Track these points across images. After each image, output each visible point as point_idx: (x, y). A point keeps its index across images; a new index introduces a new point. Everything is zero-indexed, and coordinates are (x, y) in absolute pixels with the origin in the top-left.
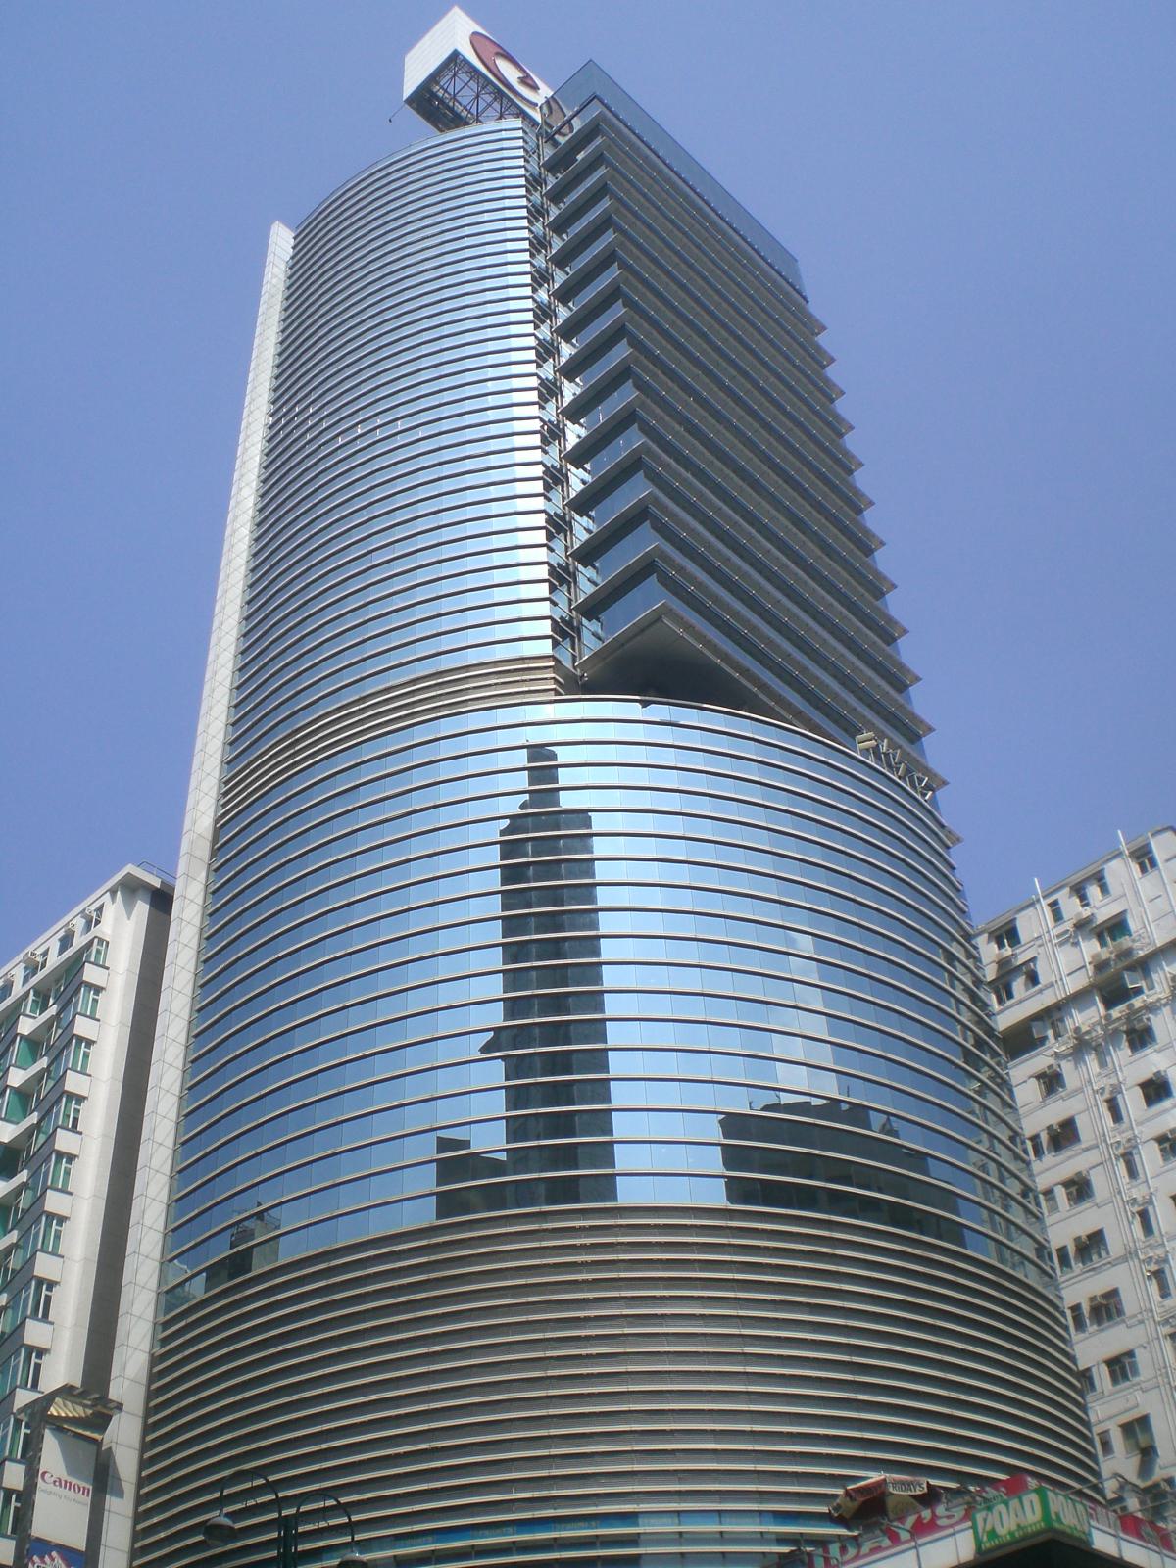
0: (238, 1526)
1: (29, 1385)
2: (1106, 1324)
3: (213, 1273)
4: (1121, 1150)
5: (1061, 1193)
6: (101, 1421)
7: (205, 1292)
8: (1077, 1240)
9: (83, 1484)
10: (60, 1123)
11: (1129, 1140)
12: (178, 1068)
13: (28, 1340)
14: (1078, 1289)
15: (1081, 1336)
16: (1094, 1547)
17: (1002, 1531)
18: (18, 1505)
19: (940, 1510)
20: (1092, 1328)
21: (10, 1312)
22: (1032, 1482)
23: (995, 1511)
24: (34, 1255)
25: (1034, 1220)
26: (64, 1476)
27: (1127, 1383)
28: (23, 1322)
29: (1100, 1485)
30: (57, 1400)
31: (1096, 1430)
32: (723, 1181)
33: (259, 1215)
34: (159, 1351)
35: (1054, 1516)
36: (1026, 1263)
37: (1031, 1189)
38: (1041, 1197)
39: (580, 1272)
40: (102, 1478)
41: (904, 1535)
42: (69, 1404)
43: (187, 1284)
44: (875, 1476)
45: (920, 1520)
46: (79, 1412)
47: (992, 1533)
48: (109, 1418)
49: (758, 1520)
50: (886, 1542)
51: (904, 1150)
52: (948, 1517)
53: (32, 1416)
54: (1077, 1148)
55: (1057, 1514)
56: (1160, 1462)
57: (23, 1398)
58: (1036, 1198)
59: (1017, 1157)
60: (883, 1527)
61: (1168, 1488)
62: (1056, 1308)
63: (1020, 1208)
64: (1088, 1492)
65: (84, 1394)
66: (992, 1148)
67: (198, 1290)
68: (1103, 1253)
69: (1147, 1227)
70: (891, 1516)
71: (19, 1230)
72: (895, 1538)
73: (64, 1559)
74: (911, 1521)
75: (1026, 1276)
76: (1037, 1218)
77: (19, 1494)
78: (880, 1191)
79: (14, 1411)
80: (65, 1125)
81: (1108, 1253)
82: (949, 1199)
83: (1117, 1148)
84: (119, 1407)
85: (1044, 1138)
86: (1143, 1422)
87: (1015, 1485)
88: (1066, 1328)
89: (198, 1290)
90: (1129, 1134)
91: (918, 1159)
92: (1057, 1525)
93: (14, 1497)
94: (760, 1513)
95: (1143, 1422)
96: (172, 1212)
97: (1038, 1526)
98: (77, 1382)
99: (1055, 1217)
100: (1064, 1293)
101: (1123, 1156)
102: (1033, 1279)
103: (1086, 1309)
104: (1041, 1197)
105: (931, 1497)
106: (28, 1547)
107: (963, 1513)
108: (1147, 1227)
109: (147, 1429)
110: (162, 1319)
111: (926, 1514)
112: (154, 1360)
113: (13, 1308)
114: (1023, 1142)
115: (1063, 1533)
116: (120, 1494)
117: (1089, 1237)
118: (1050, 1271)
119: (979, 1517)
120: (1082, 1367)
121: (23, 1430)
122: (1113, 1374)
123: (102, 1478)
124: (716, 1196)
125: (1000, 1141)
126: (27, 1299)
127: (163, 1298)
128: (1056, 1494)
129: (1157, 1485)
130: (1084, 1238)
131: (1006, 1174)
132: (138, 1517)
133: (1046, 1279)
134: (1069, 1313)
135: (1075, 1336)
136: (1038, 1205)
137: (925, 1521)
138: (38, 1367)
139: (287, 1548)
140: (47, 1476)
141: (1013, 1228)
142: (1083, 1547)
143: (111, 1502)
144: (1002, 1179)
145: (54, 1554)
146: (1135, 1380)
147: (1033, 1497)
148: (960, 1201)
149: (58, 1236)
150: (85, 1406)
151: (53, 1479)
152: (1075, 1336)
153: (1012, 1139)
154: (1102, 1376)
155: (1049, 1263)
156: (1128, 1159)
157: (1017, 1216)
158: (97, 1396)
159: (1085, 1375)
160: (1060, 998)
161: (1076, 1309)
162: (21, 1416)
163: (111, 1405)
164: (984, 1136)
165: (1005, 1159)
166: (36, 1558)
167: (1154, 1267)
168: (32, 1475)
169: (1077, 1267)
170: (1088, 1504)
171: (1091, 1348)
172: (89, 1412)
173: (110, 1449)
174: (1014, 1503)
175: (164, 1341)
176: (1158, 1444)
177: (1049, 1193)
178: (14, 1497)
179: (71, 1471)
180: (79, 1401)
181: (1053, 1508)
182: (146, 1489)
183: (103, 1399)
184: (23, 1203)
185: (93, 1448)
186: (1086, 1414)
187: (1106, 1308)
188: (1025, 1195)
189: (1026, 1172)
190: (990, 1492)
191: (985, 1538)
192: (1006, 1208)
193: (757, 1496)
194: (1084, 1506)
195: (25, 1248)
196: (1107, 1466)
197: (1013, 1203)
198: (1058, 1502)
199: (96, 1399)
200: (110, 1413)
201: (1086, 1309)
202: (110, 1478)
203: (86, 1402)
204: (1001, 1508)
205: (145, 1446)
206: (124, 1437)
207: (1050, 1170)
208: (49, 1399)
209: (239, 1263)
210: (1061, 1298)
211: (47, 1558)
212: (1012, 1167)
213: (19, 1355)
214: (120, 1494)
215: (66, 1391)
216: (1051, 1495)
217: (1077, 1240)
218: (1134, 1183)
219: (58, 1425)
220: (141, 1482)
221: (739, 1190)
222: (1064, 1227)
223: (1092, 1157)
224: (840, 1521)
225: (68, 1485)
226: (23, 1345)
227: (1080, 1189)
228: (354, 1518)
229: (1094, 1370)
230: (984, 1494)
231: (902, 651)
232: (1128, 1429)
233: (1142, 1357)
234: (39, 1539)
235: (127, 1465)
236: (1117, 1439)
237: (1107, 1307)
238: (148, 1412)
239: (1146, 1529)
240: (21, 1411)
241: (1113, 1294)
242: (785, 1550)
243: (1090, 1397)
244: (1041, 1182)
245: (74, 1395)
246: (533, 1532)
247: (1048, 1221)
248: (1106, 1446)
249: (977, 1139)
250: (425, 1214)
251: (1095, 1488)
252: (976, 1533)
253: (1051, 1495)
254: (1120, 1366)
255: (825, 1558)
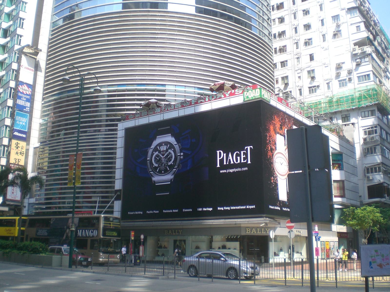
0: (71, 80)
1: (18, 44)
2: (282, 53)
3: (65, 19)
4: (293, 12)
5: (277, 20)
6: (36, 54)
7: (63, 23)
8: (279, 32)
9: (32, 68)
10: (10, 79)
11: (296, 10)
12: (46, 45)
13: (18, 33)
14: (277, 44)
15: (276, 55)
16: (270, 103)
17: (249, 97)
18: (16, 73)
19: (236, 90)
20: (278, 54)
21: (13, 26)
22: (259, 87)
23: (249, 92)
24: (19, 12)
25: (269, 26)
26: (27, 66)
27: (285, 68)
28: (17, 28)
29: (274, 90)
30: (25, 48)
31: (275, 77)
32: (195, 7)
33: (77, 5)
34: (51, 37)
35: (262, 95)
36: (266, 36)
37: (271, 33)
38: (272, 21)
39: (157, 40)
40: (37, 67)
41: (227, 95)
42: (28, 49)
43: (58, 21)
44: (222, 82)
45: (231, 92)
46: (31, 51)
47: (248, 97)
48: (38, 53)
49: (194, 89)
50: (223, 96)
51: (241, 5)
52: (238, 92)
53: (19, 51)
54: (283, 10)
55: (263, 95)
56: (289, 87)
57: (17, 47)
58: (271, 21)
59: (268, 10)
60: (223, 93)
61: (290, 93)
62: (271, 48)
63: (267, 23)
64: (271, 90)
65: (32, 47)
66: (262, 7)
67: (61, 23)
68: (284, 36)
69: (296, 32)
70: (225, 91)
71: (6, 71)
72: (225, 96)
73: (27, 86)
74: (229, 92)
75: (265, 39)
76: (270, 25)
77: (16, 71)
78: (233, 14)
79: (15, 50)
80: (12, 79)
81: (286, 36)
82: (249, 18)
83: (292, 11)
84: (41, 50)
85: (275, 6)
86: (287, 77)
87: (254, 87)
88: (272, 53)
89: (61, 23)
90: (296, 8)
91: (244, 8)
92: (263, 97)
93: (15, 71)
94: (195, 87)
95: (287, 77)
96: (54, 3)
97: (266, 265)
98: (30, 43)
99: (275, 26)
100: (273, 44)
101: (294, 13)
102: (267, 40)
103: (278, 49)
104: (272, 21)
105: (233, 87)
106: (18, 83)
107: (241, 92)
108: (296, 32)
109: (48, 56)
110: (52, 29)
111: (233, 91)
112: (50, 39)
113: (14, 25)
114: (270, 7)
115: (264, 99)
116: (41, 71)
117: (282, 32)
118: (271, 39)
119: (245, 93)
120: (274, 62)
121: (17, 55)
122: (282, 65)
123: (37, 67)
124: (192, 11)
125: (264, 6)
126: (17, 23)
127: (52, 24)
128: (264, 90)
129: (287, 92)
130: (280, 32)
131: (264, 14)
132: (46, 77)
133: (270, 41)
134: (274, 50)
135: (274, 55)
136: (271, 22)
137: (232, 93)
138: (20, 40)
139: (81, 91)
140: (23, 66)
141: (263, 5)
142: (268, 103)
143: (39, 73)
144: (263, 15)
145: (25, 85)
146: (286, 67)
147: (258, 90)
148: (252, 19)
149: (25, 7)
150: (32, 50)
151: (24, 67)
152: (274, 55)
153: (268, 5)
154: (279, 65)
155: (271, 37)
156: (295, 14)
157: (265, 24)
158: (35, 47)
159: (275, 65)
160: (310, 282)
161: (276, 49)
162: (16, 52)
163: (39, 50)
164: (261, 4)
165: (265, 10)
166: (20, 86)
167: (296, 41)
168: (19, 66)
169: (278, 39)
170: (271, 93)
171: (277, 58)
172: (33, 51)
173: (38, 60)
174: (254, 91)
175: (52, 35)
176: (289, 83)
177: (274, 20)
178: (15, 71)
179: (29, 65)
180: (31, 48)
181: (262, 93)
182: (48, 70)
183: (37, 48)
184: (9, 45)
185: (34, 60)
186: (274, 73)
187: (283, 50)
188: (268, 20)
189: (269, 14)
190: (249, 88)
191: (246, 98)
192: (263, 22)
193: (194, 83)
194: (270, 94)
195: (17, 10)
196: (276, 86)
197: (265, 21)
198: (264, 92)
199: (35, 48)
200: (38, 52)
201: (278, 49)
202: (38, 68)
203: (32, 49)
204: (251, 91)
205: (48, 60)
206: (42, 58)
207: (275, 14)
208: (23, 48)
209: (71, 17)
210: (272, 46)
211: (23, 86)
212: (266, 12)
213: (18, 20)
214: (41, 71)
215: (28, 46)
216: (262, 90)
217: (279, 32)
218: (295, 20)
219: (26, 54)
220: (47, 69)
221: (199, 10)
222: (276, 29)
223: (286, 13)
224: (212, 90)
225: (28, 69)
226: (19, 17)
227: (282, 20)
228: (98, 80)
229: (277, 64)
230: (247, 88)
231: (280, 254)
232: (283, 78)
233: (289, 62)
234: (21, 82)
235: (43, 64)
236: (280, 80)
237: (283, 49)
238: (48, 52)
239: (283, 101)
240: (17, 50)
241: (285, 46)
242: (199, 96)
243: (275, 70)
244: (272, 18)
245: (30, 47)
246: (141, 86)
247: (273, 27)
248: (277, 82)
249: (259, 4)
250: (119, 8)
251: (272, 90)
252: (244, 96)
253: (262, 90)
254: (283, 64)
255: (208, 98)
